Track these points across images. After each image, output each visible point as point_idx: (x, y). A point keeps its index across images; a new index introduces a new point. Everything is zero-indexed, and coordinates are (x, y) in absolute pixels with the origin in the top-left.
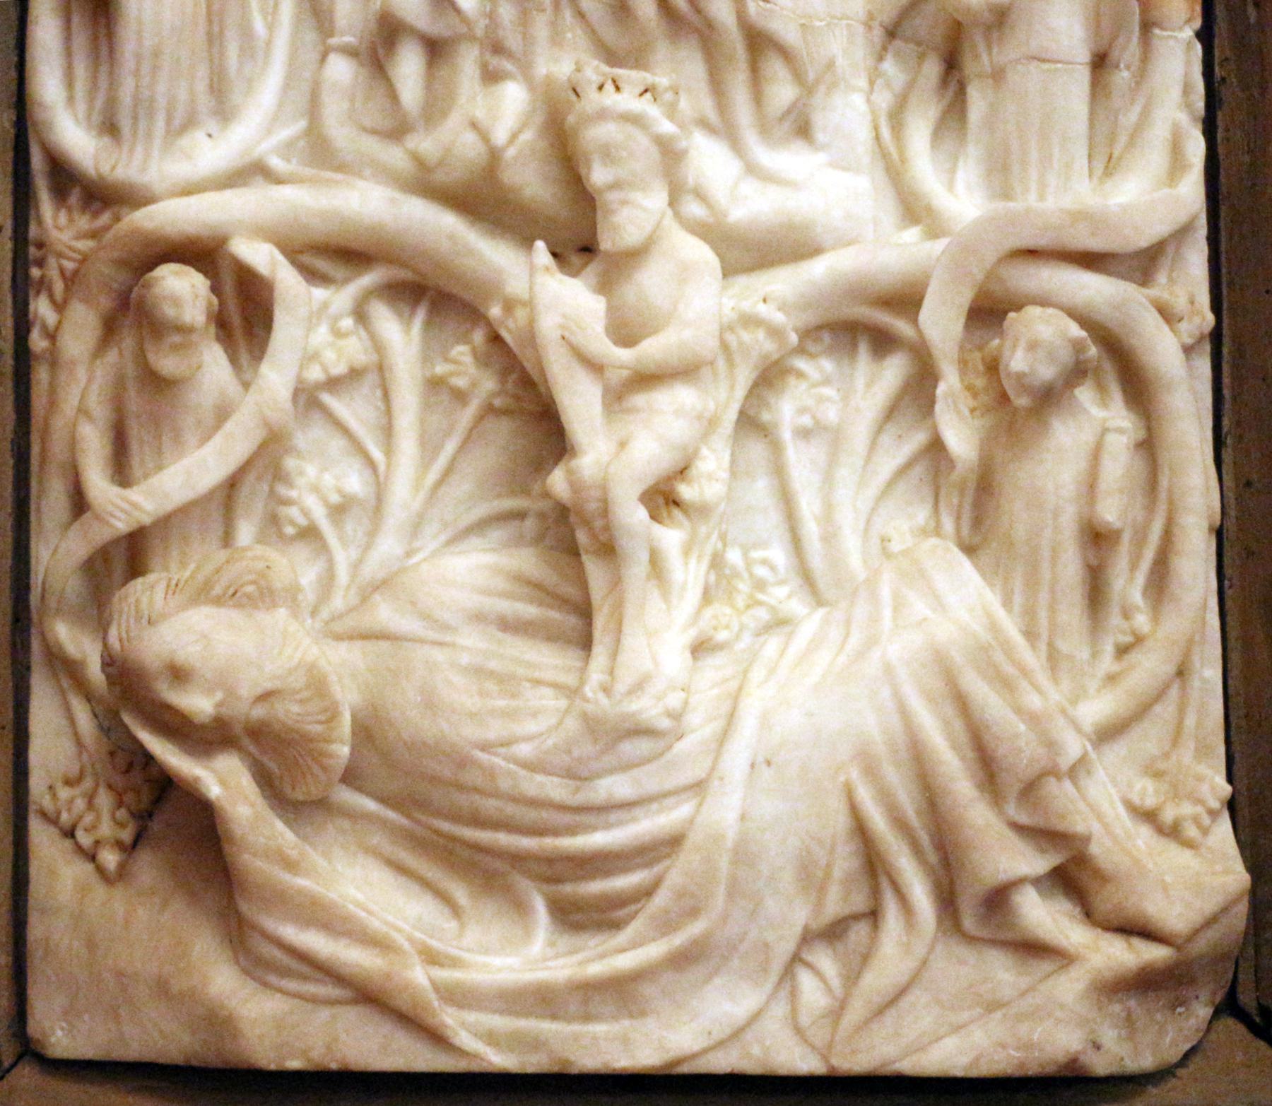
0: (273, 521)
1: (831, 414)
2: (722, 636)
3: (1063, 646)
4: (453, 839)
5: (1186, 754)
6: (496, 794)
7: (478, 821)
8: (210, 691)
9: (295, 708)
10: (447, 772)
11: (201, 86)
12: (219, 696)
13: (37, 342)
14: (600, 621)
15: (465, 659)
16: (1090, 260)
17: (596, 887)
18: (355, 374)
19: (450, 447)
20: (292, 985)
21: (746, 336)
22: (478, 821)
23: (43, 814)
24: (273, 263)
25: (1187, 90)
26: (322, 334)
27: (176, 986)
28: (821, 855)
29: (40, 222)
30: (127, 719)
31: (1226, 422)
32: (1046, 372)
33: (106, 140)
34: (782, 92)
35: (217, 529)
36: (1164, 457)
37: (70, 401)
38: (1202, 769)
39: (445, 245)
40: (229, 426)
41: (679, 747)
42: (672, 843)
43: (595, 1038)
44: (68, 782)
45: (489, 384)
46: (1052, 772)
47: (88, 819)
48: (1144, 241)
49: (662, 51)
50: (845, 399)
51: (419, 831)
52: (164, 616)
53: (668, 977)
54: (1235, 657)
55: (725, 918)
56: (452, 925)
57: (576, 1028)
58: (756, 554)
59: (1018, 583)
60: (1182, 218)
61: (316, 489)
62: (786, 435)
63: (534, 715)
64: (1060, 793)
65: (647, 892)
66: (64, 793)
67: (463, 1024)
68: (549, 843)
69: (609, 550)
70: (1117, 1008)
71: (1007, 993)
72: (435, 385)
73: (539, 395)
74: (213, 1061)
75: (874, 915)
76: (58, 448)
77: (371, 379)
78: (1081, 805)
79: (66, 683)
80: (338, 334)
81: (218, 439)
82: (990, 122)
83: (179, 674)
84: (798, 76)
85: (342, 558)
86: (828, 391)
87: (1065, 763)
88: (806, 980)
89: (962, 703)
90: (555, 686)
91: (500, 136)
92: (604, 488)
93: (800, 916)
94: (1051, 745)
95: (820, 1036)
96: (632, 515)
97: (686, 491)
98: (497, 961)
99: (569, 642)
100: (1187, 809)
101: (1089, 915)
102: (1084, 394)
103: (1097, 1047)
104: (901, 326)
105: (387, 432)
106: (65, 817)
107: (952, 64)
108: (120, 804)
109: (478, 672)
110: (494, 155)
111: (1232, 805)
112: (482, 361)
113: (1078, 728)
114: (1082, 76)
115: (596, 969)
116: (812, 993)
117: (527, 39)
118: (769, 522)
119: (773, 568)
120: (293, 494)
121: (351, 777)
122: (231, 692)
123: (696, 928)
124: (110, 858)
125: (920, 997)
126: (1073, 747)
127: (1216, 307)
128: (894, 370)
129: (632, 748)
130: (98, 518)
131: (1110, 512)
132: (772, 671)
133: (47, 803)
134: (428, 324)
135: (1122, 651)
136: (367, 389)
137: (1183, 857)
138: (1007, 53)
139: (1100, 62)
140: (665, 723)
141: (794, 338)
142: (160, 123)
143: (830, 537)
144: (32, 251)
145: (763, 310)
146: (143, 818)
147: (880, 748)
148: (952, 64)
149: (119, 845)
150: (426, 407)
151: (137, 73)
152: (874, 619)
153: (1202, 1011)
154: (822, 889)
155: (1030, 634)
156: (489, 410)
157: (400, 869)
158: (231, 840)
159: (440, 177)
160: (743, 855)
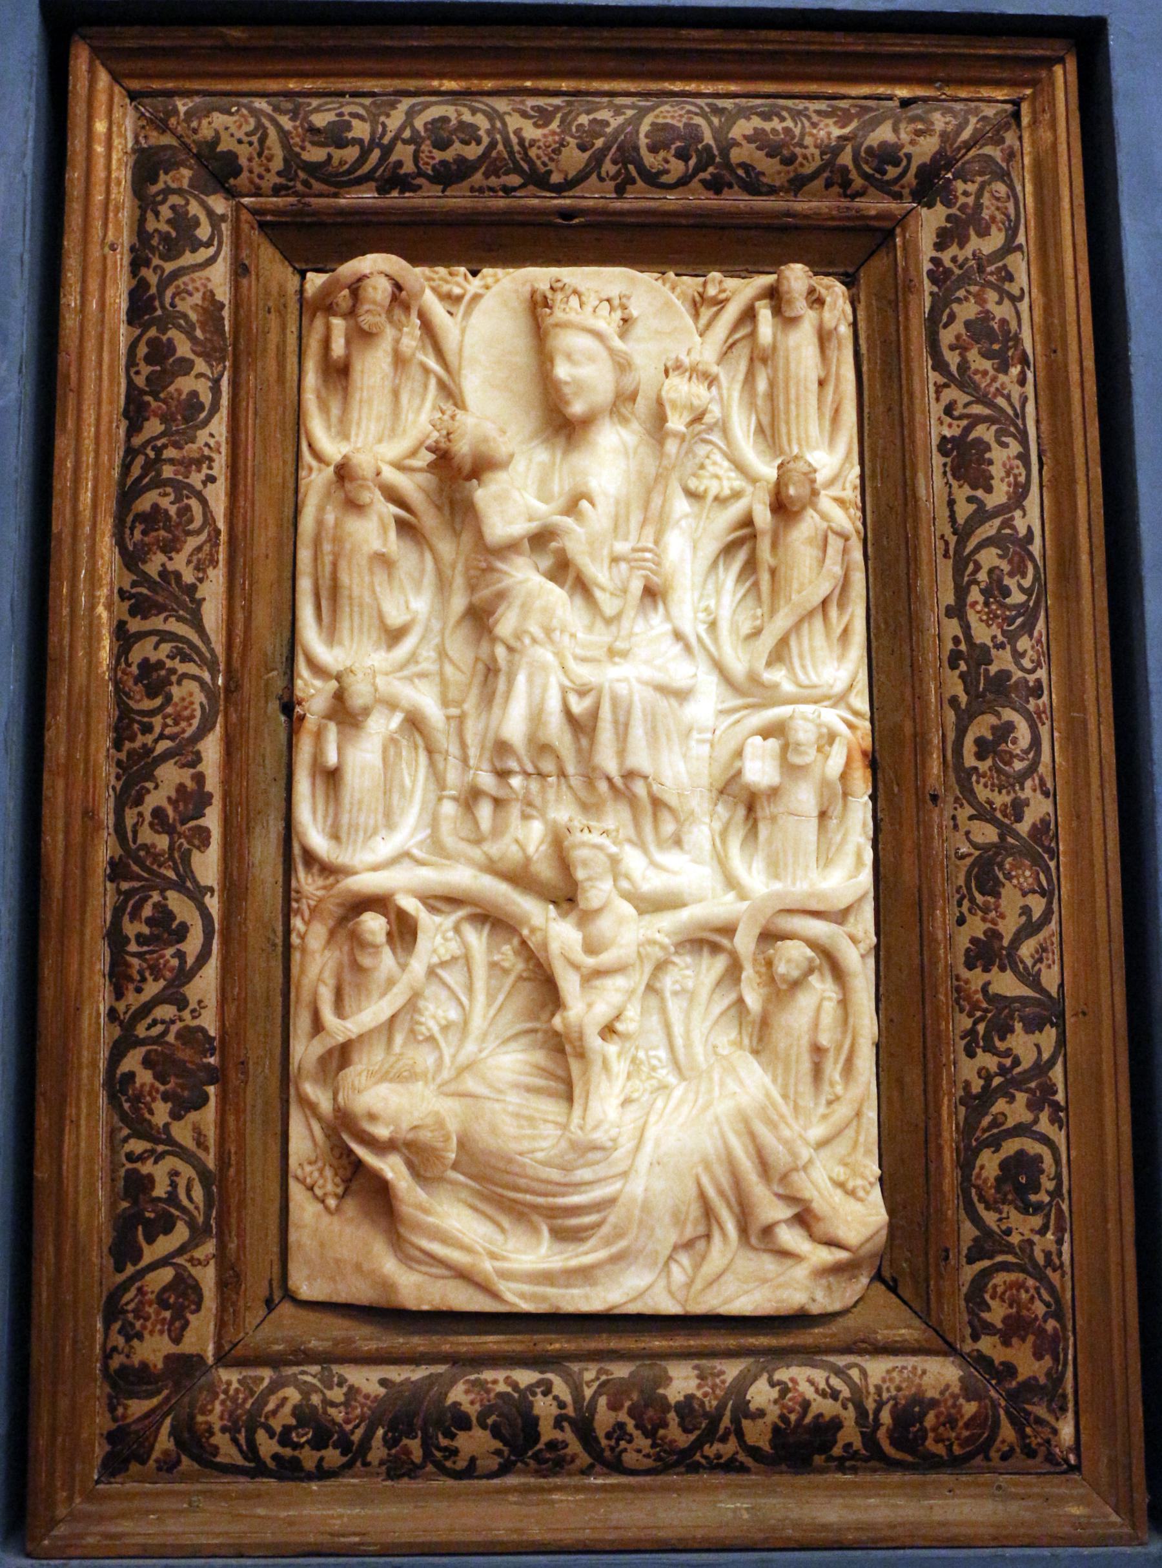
0: (412, 1031)
1: (690, 984)
2: (635, 1095)
3: (801, 1103)
4: (501, 1196)
5: (859, 1155)
6: (526, 1176)
7: (516, 1188)
8: (387, 1125)
9: (429, 1135)
10: (501, 1165)
11: (380, 817)
12: (392, 1128)
13: (295, 940)
14: (577, 1092)
15: (511, 1108)
16: (816, 914)
17: (574, 1222)
18: (454, 959)
19: (501, 998)
20: (424, 1268)
21: (649, 949)
22: (516, 1188)
23: (297, 1178)
24: (417, 909)
25: (864, 825)
26: (439, 939)
27: (366, 1267)
28: (684, 1209)
29: (298, 881)
30: (345, 1137)
31: (881, 989)
32: (795, 974)
33: (333, 843)
34: (668, 827)
35: (384, 1039)
36: (851, 1011)
37: (313, 971)
38: (867, 1162)
39: (501, 900)
40: (395, 990)
41: (617, 1154)
42: (611, 1202)
43: (572, 1297)
44: (310, 1163)
45: (520, 966)
46: (796, 1169)
47: (321, 1182)
48: (843, 906)
49: (610, 807)
50: (697, 975)
51: (486, 1192)
52: (366, 1088)
53: (608, 1267)
54: (884, 1106)
55: (636, 1239)
56: (499, 1238)
57: (562, 1291)
58: (652, 1053)
59: (780, 1071)
60: (861, 892)
61: (434, 1017)
62: (668, 995)
63: (545, 1138)
64: (799, 1178)
65: (598, 1225)
66: (308, 1169)
67: (509, 1290)
68: (551, 1200)
69: (582, 1055)
70: (824, 1282)
71: (770, 1275)
72: (493, 965)
73: (545, 971)
74: (383, 1303)
75: (708, 1236)
76: (306, 996)
77: (462, 962)
78: (809, 1185)
79: (308, 1113)
80: (446, 939)
81: (388, 997)
82: (770, 841)
83: (372, 1117)
84: (676, 819)
85: (447, 1052)
86: (688, 972)
87: (800, 1163)
88: (674, 1268)
89: (752, 1136)
90: (556, 1123)
91: (531, 850)
92: (581, 1026)
93: (673, 1237)
94: (794, 1155)
95: (681, 1295)
96: (594, 1042)
97: (619, 1027)
98: (524, 1257)
99: (561, 1097)
100: (859, 1182)
101: (812, 1236)
102: (814, 979)
103: (814, 1300)
104: (725, 942)
105: (470, 989)
106: (308, 1180)
107: (751, 808)
108: (336, 1174)
109: (517, 1116)
110: (528, 860)
111: (881, 1179)
112: (517, 953)
113: (807, 1143)
114: (815, 822)
115: (574, 1263)
116: (678, 1275)
117: (545, 801)
118: (659, 1037)
119: (660, 1060)
120: (423, 1019)
121: (455, 1166)
122: (397, 1127)
123: (621, 1244)
124: (332, 1202)
125: (728, 1277)
126: (805, 1153)
127: (877, 934)
128: (720, 963)
129: (592, 1156)
130: (328, 1034)
131: (824, 1040)
132: (661, 1115)
133: (299, 1173)
134: (490, 935)
135: (830, 1103)
136: (459, 968)
137: (857, 1207)
138: (778, 808)
139: (823, 815)
140: (609, 1144)
141: (672, 949)
142: (361, 834)
143: (688, 1045)
144: (293, 895)
145: (658, 937)
146: (347, 1181)
147: (713, 1157)
148: (751, 808)
149: (336, 1195)
150: (490, 977)
151: (350, 811)
152: (710, 1091)
153: (864, 1280)
154: (684, 1223)
155: (785, 1096)
156: (520, 978)
157: (475, 1209)
158: (396, 1196)
159: (500, 866)
160: (646, 1208)
